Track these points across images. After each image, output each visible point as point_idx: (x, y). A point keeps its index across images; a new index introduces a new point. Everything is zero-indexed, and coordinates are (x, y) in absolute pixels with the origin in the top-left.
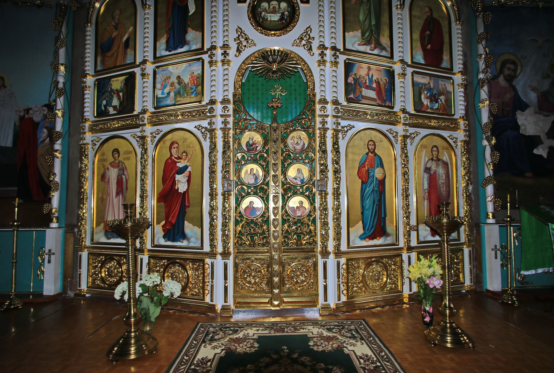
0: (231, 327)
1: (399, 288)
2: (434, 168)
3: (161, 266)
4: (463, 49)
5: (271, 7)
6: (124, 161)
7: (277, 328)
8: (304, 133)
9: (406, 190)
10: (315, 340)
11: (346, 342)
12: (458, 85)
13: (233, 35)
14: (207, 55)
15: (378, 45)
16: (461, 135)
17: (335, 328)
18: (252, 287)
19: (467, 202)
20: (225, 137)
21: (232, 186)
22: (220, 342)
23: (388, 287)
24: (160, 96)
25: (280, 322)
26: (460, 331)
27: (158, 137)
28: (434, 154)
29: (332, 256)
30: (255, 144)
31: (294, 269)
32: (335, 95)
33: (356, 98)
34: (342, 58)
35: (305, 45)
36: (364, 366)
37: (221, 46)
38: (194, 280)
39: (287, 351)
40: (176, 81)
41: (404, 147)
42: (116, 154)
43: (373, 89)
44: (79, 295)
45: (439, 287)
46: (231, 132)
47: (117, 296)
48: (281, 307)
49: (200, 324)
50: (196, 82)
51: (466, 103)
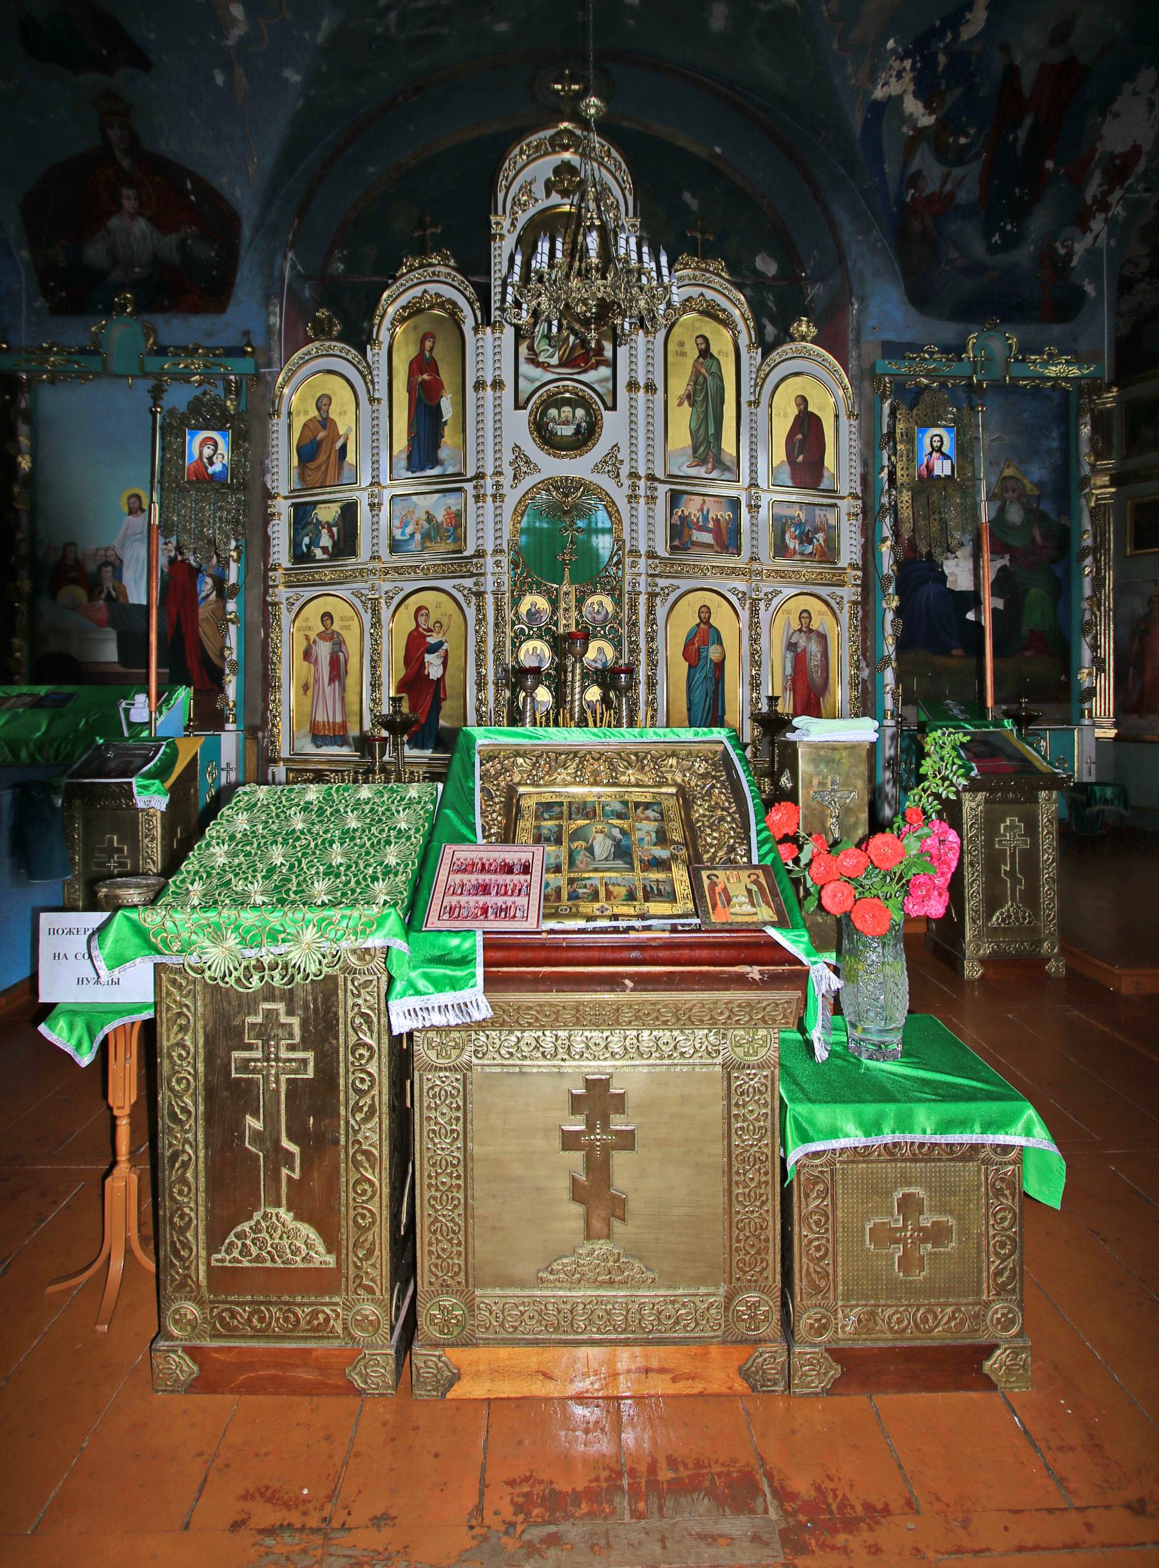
2: (802, 643)
13: (508, 456)
16: (849, 593)
24: (398, 537)
34: (662, 490)
43: (709, 531)
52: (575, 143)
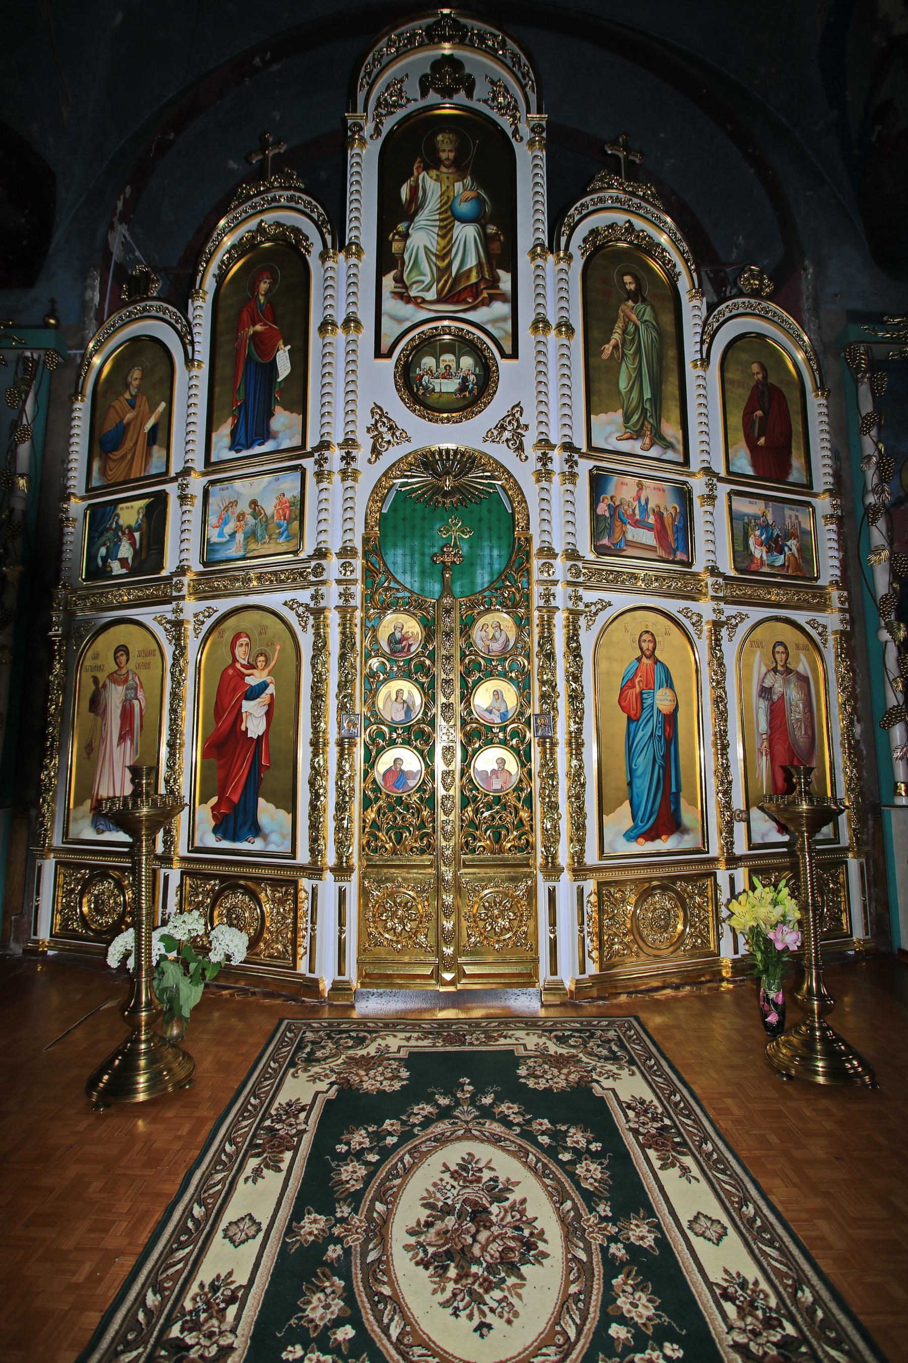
0: (352, 1031)
1: (712, 945)
2: (778, 688)
3: (206, 894)
4: (831, 445)
5: (442, 366)
6: (137, 672)
7: (449, 1035)
8: (506, 616)
9: (721, 736)
10: (531, 1064)
11: (598, 1070)
12: (825, 517)
14: (312, 459)
15: (658, 438)
16: (833, 620)
17: (574, 1036)
18: (398, 942)
19: (851, 761)
20: (344, 625)
21: (358, 726)
22: (327, 1066)
23: (687, 945)
24: (215, 539)
25: (457, 1021)
26: (843, 1047)
27: (209, 622)
28: (778, 660)
29: (566, 876)
30: (407, 639)
31: (487, 904)
32: (571, 539)
33: (614, 545)
34: (584, 467)
35: (510, 440)
36: (636, 1126)
37: (341, 441)
38: (276, 924)
39: (471, 1088)
40: (248, 511)
41: (716, 643)
42: (122, 655)
44: (34, 952)
45: (796, 949)
46: (359, 614)
47: (113, 961)
48: (459, 987)
49: (286, 1022)
50: (288, 512)
51: (841, 554)
52: (460, 36)
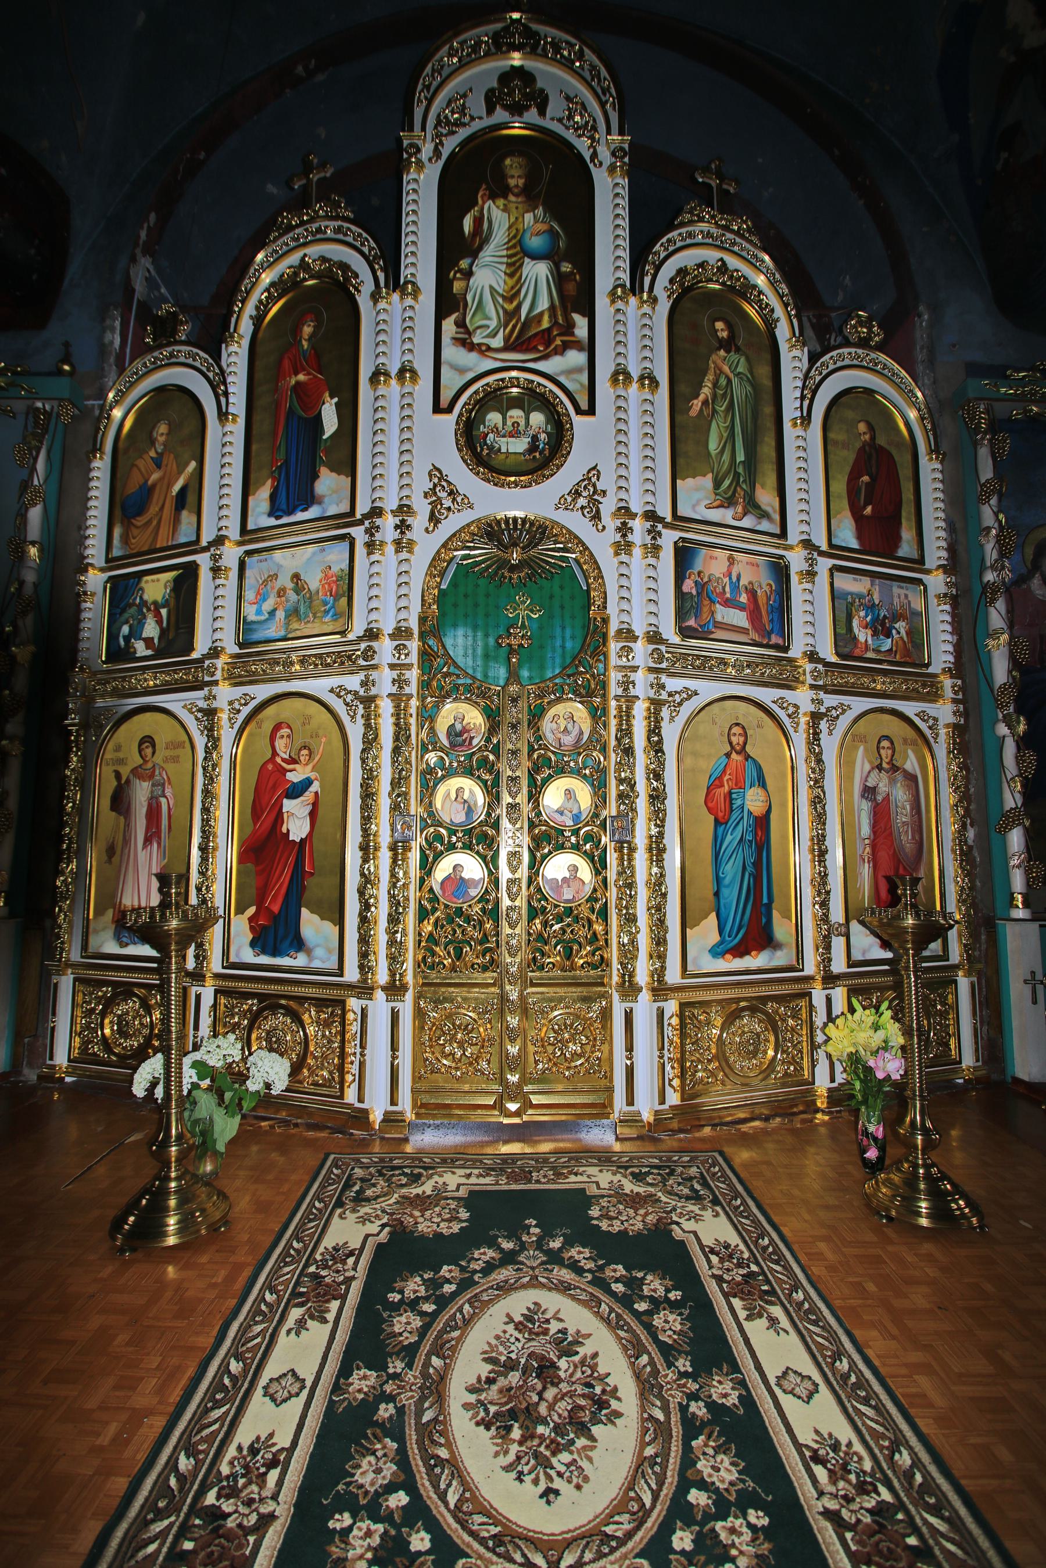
2: (883, 788)
13: (422, 483)
16: (945, 712)
24: (252, 617)
34: (669, 538)
43: (742, 609)
52: (531, 45)
